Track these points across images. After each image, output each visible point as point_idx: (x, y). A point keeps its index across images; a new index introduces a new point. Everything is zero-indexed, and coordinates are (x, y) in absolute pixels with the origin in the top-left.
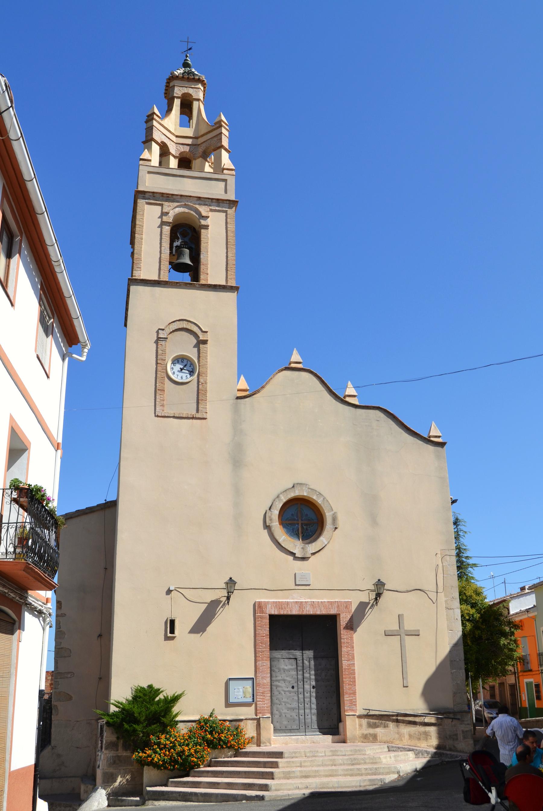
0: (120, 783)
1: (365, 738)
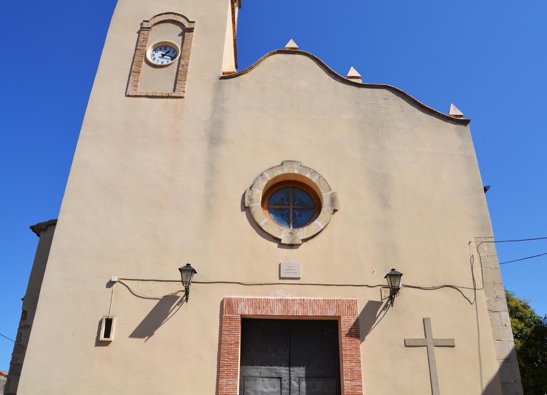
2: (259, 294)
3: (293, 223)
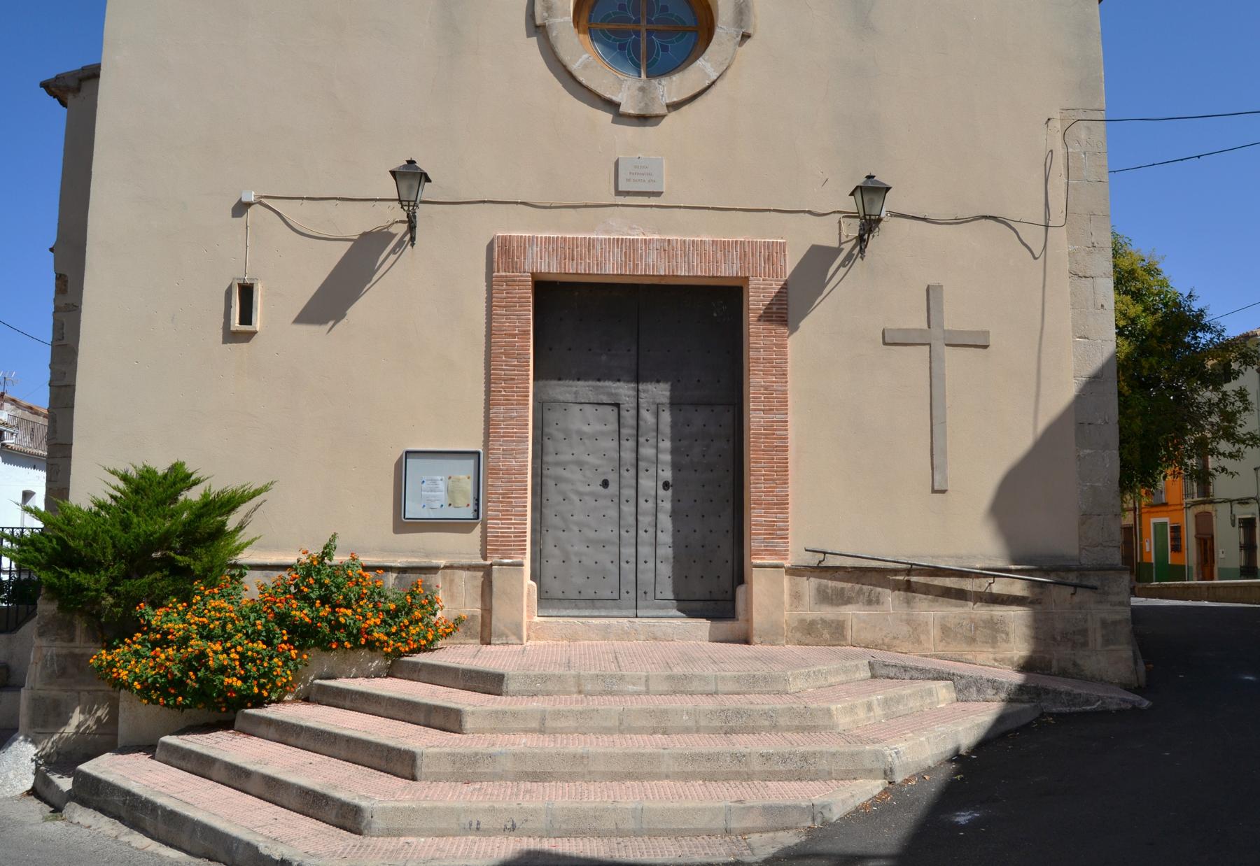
0: (78, 727)
1: (809, 632)
2: (571, 228)
3: (648, 66)
